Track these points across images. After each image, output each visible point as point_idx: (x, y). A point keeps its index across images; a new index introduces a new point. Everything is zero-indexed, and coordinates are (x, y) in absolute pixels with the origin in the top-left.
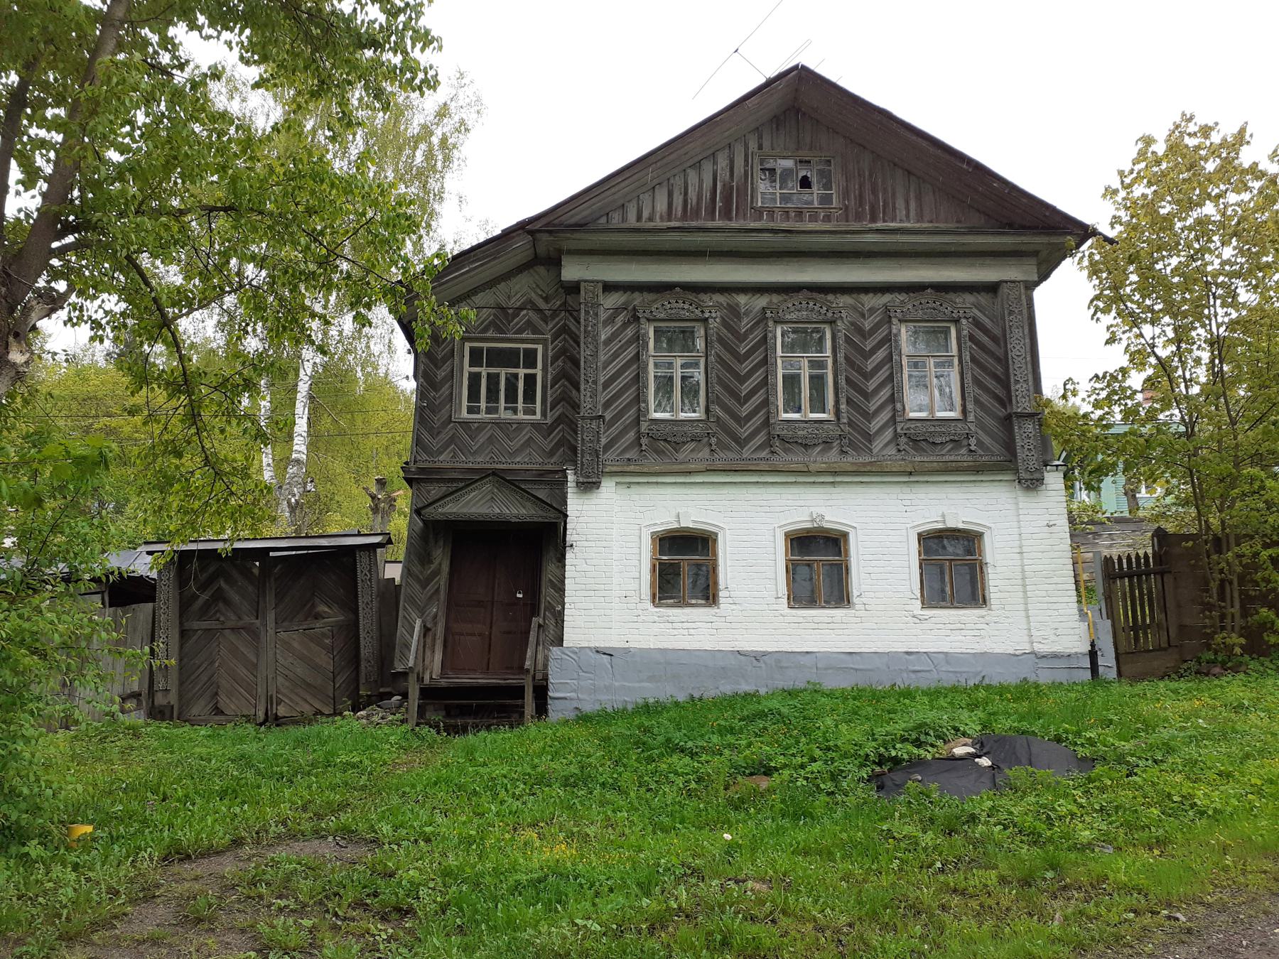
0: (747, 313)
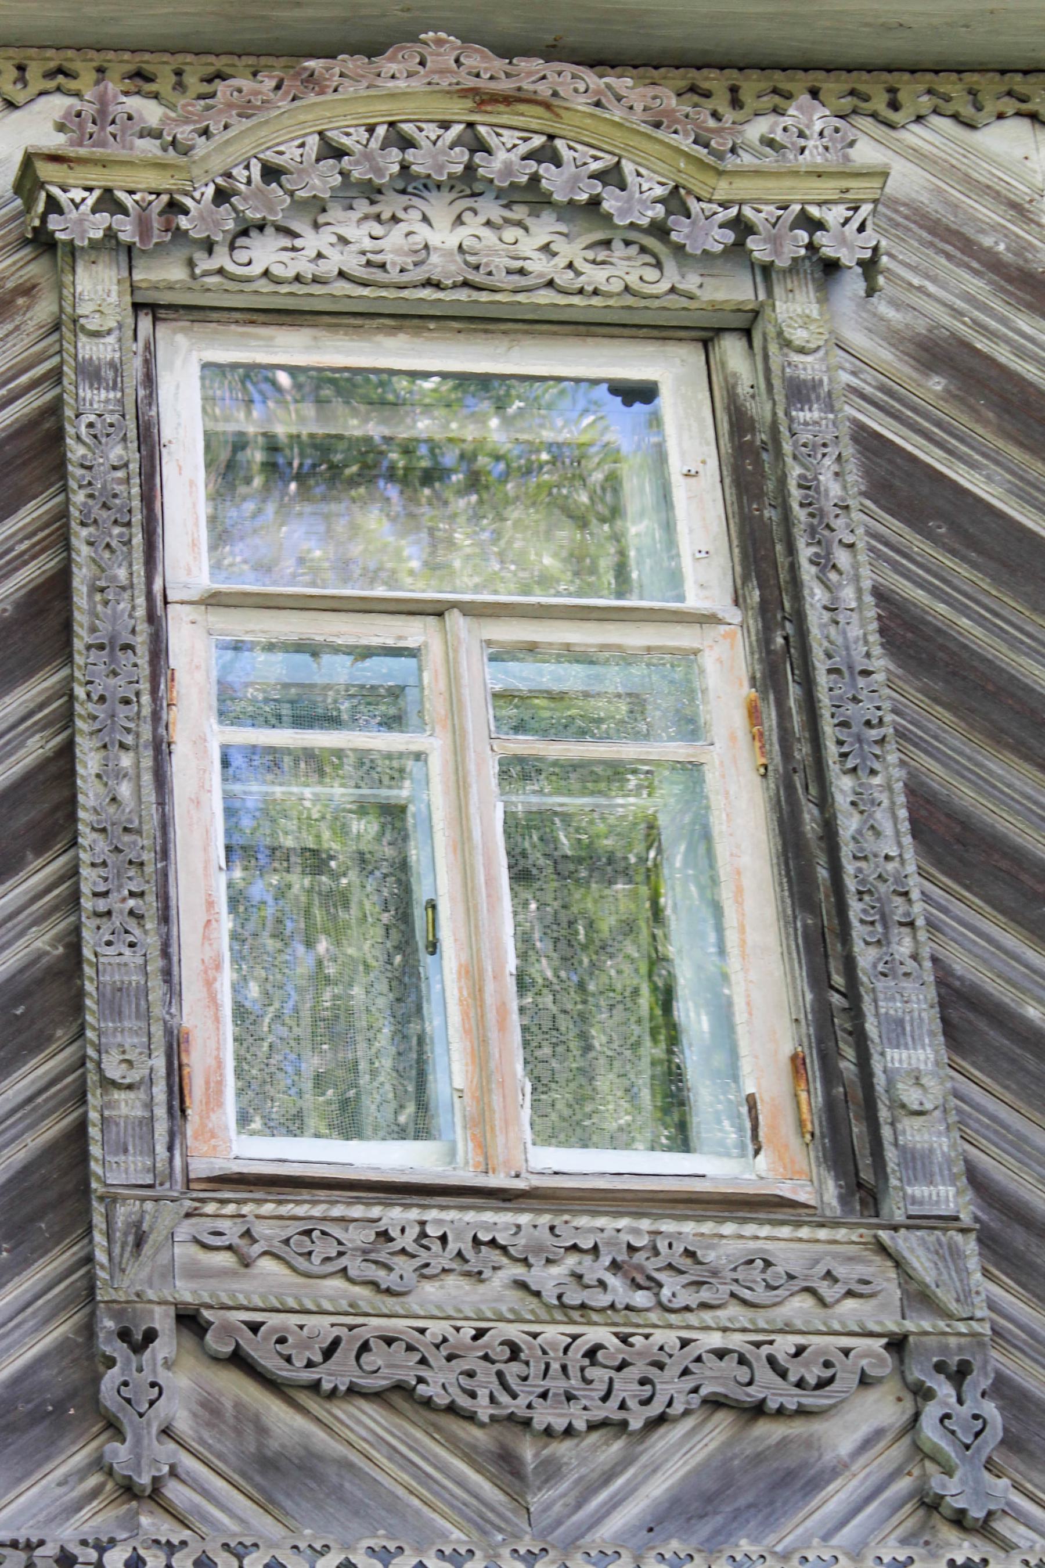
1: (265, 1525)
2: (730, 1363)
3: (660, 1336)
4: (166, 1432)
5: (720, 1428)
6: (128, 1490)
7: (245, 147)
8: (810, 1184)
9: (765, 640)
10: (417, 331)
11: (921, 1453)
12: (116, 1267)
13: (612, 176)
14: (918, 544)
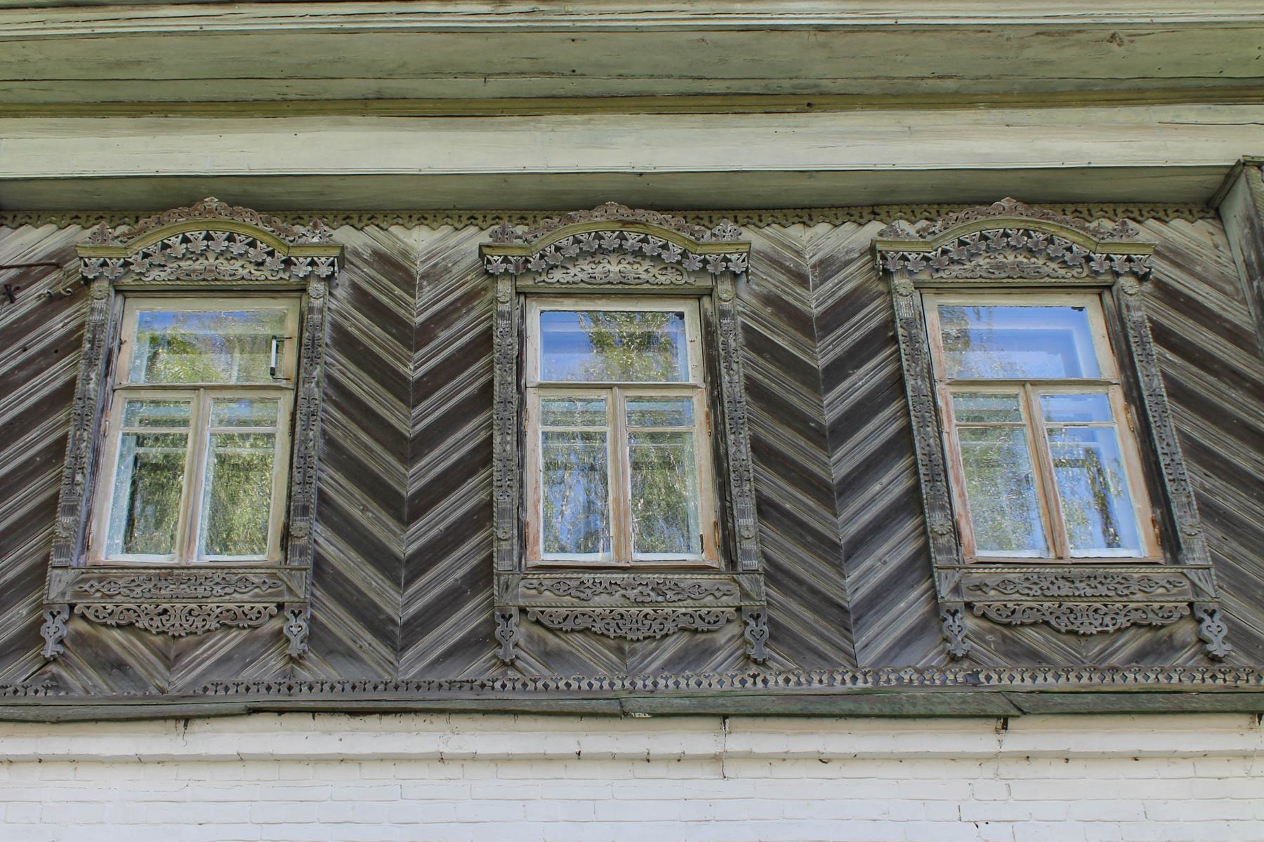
0: (432, 276)
1: (546, 672)
2: (1140, 613)
3: (666, 610)
4: (516, 645)
5: (684, 639)
6: (504, 664)
7: (549, 241)
8: (717, 561)
9: (712, 393)
10: (608, 299)
11: (746, 642)
12: (500, 596)
13: (665, 247)
14: (761, 361)
